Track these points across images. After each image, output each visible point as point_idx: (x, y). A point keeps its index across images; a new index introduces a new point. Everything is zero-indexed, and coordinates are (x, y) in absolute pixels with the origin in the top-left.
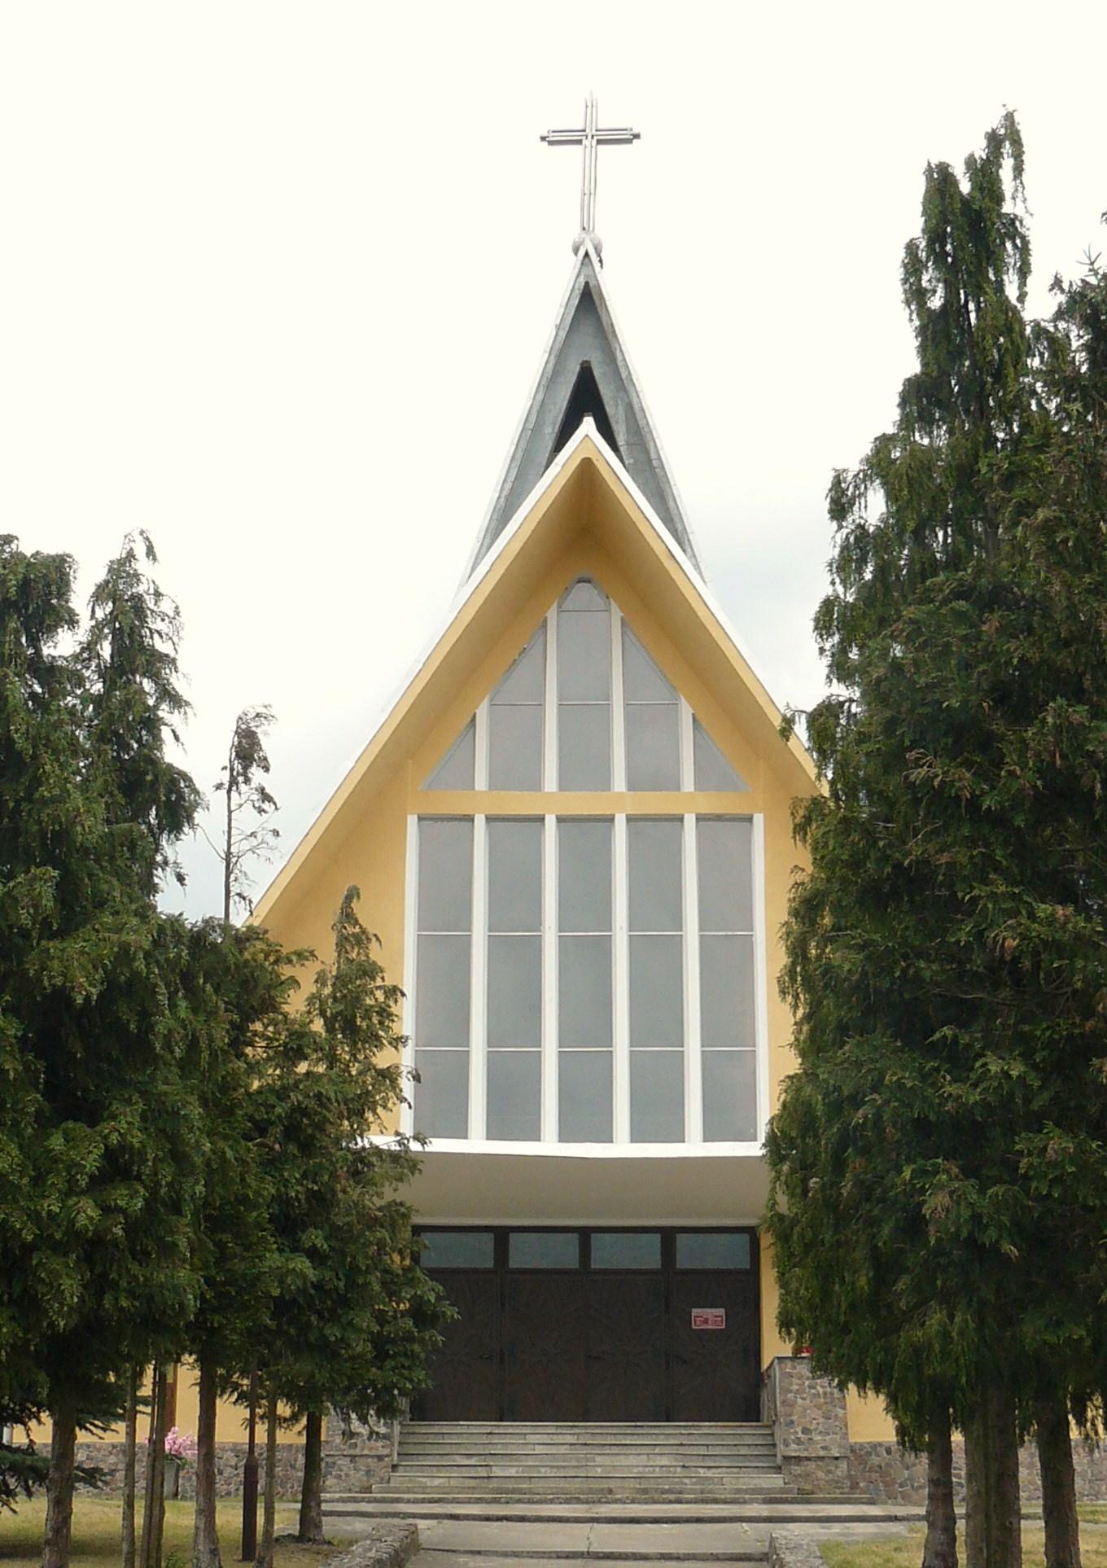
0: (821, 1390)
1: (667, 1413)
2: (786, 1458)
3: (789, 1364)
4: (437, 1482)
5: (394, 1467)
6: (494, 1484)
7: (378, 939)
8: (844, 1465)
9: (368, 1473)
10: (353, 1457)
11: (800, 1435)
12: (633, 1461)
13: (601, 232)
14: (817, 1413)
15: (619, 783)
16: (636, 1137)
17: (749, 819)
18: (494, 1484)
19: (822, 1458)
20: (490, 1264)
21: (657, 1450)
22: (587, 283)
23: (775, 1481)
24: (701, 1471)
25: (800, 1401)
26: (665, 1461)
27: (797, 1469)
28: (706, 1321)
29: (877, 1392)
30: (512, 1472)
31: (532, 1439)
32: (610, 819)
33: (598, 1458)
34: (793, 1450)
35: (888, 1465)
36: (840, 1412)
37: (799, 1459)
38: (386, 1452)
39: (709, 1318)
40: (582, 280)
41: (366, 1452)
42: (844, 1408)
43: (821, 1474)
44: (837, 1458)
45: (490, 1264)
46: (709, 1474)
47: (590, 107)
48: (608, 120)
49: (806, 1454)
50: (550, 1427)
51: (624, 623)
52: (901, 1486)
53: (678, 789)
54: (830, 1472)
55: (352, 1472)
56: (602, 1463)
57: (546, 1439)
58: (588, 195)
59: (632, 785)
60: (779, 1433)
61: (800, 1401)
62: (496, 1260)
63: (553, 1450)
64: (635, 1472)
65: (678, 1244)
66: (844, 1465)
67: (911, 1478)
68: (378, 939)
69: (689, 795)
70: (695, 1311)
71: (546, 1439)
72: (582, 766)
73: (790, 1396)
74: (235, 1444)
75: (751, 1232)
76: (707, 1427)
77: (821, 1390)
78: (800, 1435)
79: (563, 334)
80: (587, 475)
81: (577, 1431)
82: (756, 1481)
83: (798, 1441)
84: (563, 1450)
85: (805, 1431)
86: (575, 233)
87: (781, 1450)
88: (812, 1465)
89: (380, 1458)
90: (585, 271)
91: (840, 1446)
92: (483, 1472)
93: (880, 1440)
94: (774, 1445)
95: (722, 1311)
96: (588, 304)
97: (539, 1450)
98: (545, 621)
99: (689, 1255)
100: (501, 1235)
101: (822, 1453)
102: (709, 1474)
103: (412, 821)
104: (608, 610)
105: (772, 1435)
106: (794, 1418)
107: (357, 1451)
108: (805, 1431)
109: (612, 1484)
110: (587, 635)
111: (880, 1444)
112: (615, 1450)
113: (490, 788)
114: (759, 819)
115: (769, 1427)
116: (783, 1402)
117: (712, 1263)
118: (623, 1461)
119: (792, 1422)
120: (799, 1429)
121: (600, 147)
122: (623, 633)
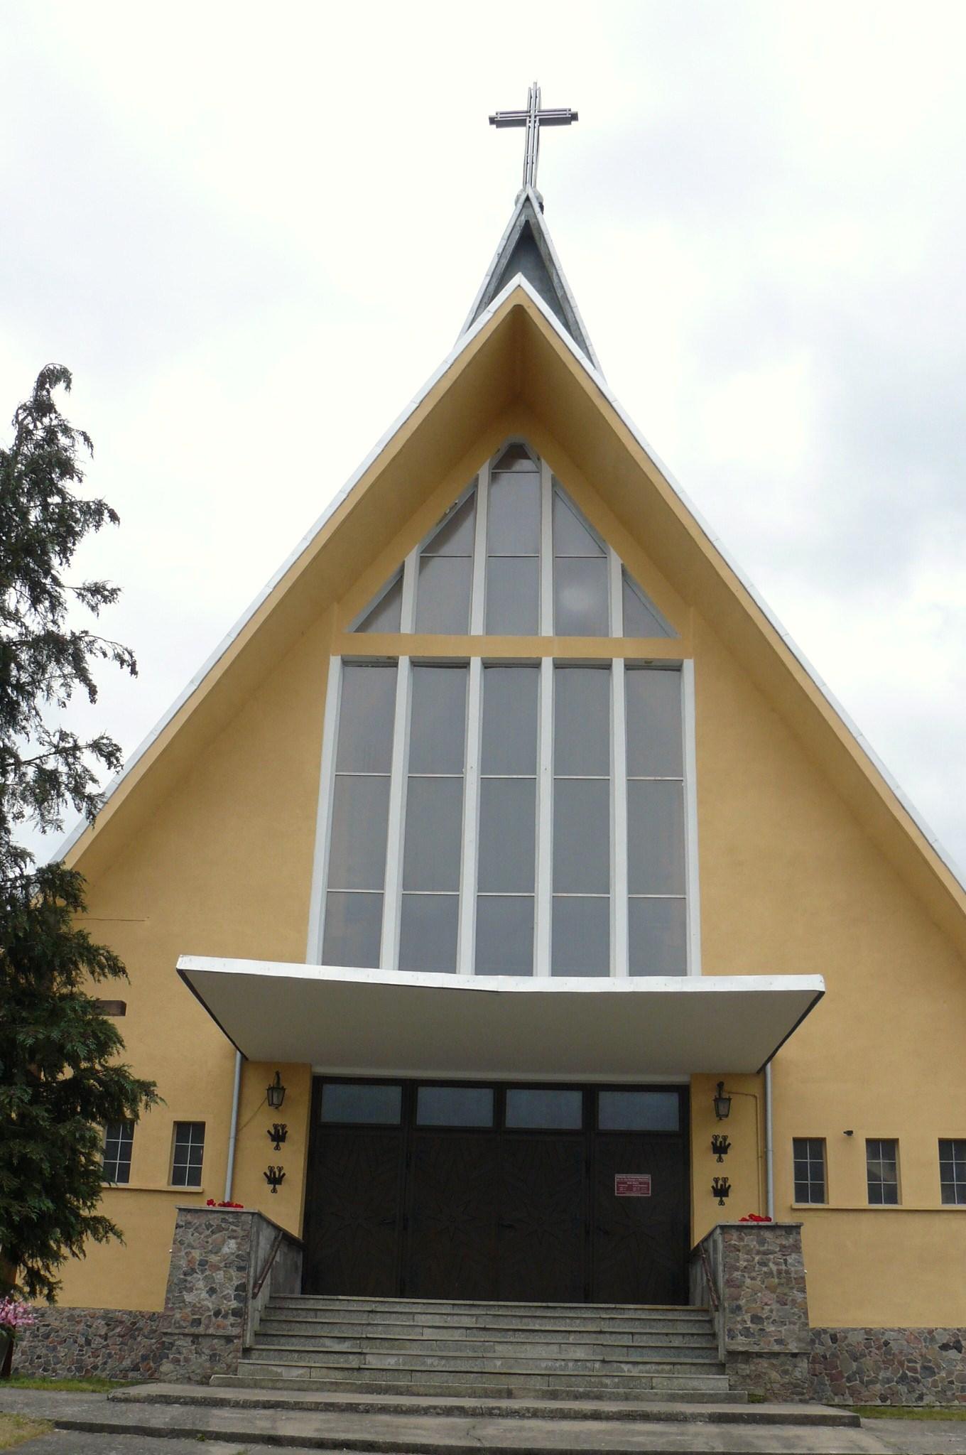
0: (774, 1268)
1: (585, 1292)
2: (732, 1354)
3: (735, 1235)
4: (295, 1373)
5: (247, 1352)
6: (366, 1378)
7: (87, 439)
8: (804, 1364)
9: (213, 1357)
10: (196, 1338)
11: (749, 1324)
12: (542, 1352)
13: (545, 186)
14: (770, 1297)
15: (547, 629)
16: (558, 969)
17: (678, 668)
18: (366, 1378)
19: (779, 1354)
20: (396, 1120)
21: (572, 1339)
22: (527, 222)
23: (719, 1383)
24: (625, 1367)
25: (748, 1281)
26: (580, 1353)
27: (745, 1369)
28: (630, 1188)
29: (56, 1256)
30: (390, 1362)
31: (421, 1320)
32: (537, 665)
33: (498, 1348)
34: (741, 1343)
35: (834, 1355)
36: (799, 1296)
37: (747, 1356)
38: (235, 1331)
39: (635, 1184)
40: (523, 218)
41: (211, 1331)
42: (803, 1290)
43: (774, 1375)
44: (794, 1355)
45: (396, 1120)
46: (635, 1371)
47: (534, 96)
48: (549, 103)
49: (756, 1349)
50: (445, 1306)
51: (554, 483)
52: (849, 1380)
53: (606, 634)
54: (786, 1372)
55: (193, 1357)
56: (503, 1354)
57: (438, 1321)
58: (530, 165)
59: (560, 629)
60: (719, 1320)
61: (748, 1281)
62: (403, 1117)
63: (445, 1335)
64: (543, 1367)
65: (601, 1102)
66: (804, 1364)
67: (859, 1372)
68: (87, 439)
69: (617, 638)
70: (618, 1177)
71: (438, 1321)
72: (511, 606)
73: (737, 1274)
74: (107, 1311)
75: (683, 1092)
76: (632, 1311)
77: (774, 1268)
78: (749, 1324)
79: (504, 262)
80: (518, 320)
81: (474, 1312)
82: (695, 1383)
83: (747, 1333)
84: (457, 1335)
85: (756, 1319)
86: (515, 186)
87: (724, 1343)
88: (764, 1363)
89: (229, 1339)
90: (529, 211)
91: (800, 1340)
92: (354, 1362)
93: (824, 1326)
94: (714, 1335)
95: (646, 1178)
96: (527, 248)
97: (428, 1334)
98: (477, 479)
99: (617, 1114)
100: (410, 1087)
101: (776, 1348)
102: (635, 1371)
103: (335, 663)
104: (539, 472)
105: (711, 1322)
106: (742, 1302)
107: (201, 1330)
108: (756, 1319)
109: (514, 1383)
110: (520, 509)
111: (825, 1331)
112: (521, 1337)
113: (416, 632)
114: (689, 666)
115: (706, 1311)
116: (729, 1283)
117: (639, 1124)
118: (530, 1352)
119: (739, 1308)
120: (747, 1317)
121: (545, 130)
122: (555, 494)
